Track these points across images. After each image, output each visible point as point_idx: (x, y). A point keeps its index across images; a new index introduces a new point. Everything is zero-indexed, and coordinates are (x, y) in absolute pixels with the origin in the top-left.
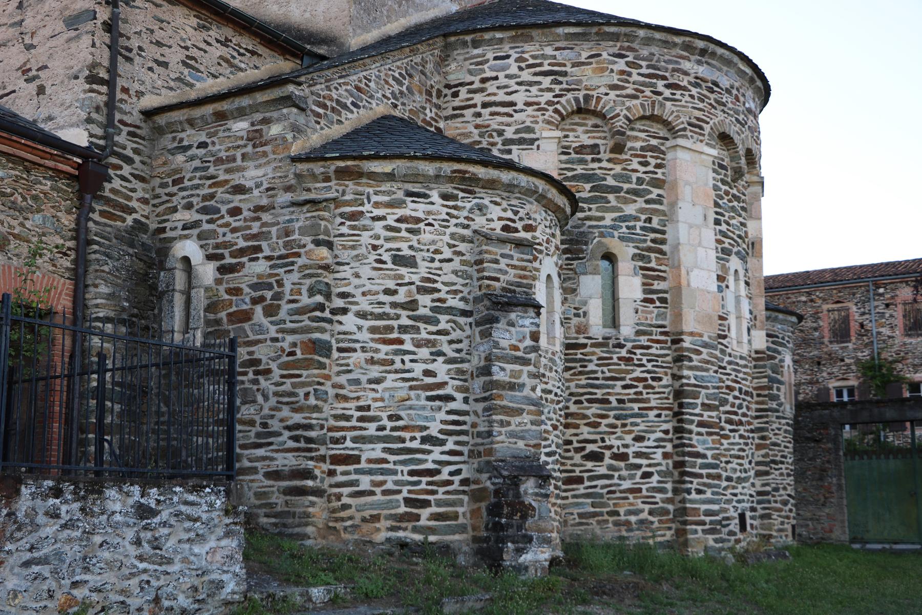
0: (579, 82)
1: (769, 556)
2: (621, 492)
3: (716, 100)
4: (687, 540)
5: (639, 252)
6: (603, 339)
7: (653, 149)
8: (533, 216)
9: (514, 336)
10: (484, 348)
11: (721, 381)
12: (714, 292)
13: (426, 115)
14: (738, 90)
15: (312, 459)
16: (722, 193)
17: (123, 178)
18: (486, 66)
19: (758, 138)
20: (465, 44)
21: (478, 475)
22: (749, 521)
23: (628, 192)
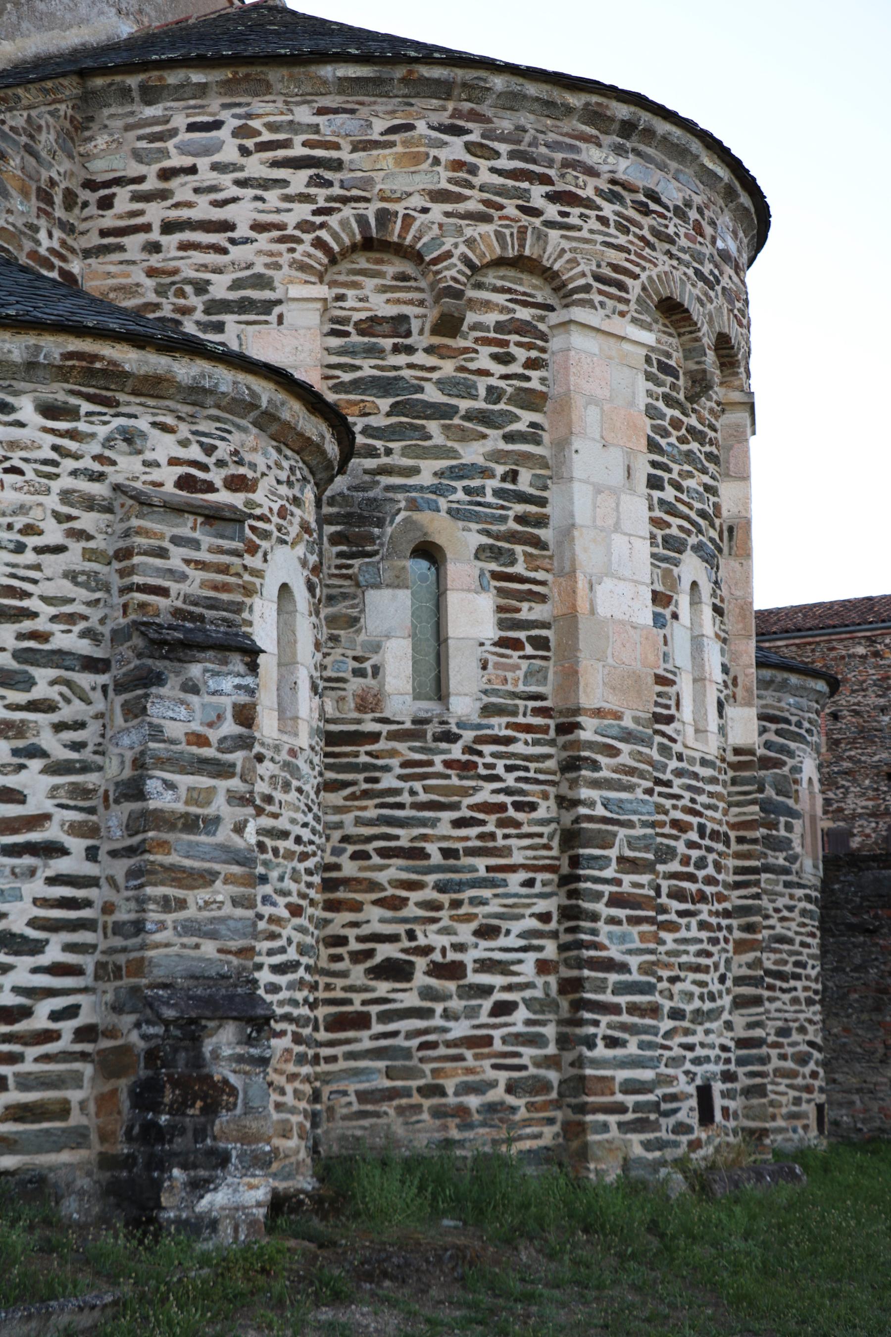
0: (367, 183)
1: (760, 1177)
2: (449, 1044)
3: (654, 231)
4: (585, 1146)
5: (490, 541)
6: (414, 722)
7: (522, 328)
8: (248, 457)
9: (198, 715)
10: (130, 741)
11: (660, 809)
12: (645, 627)
13: (38, 243)
14: (700, 211)
16: (666, 423)
18: (170, 144)
19: (743, 313)
20: (125, 94)
21: (113, 1019)
22: (718, 1102)
23: (468, 417)
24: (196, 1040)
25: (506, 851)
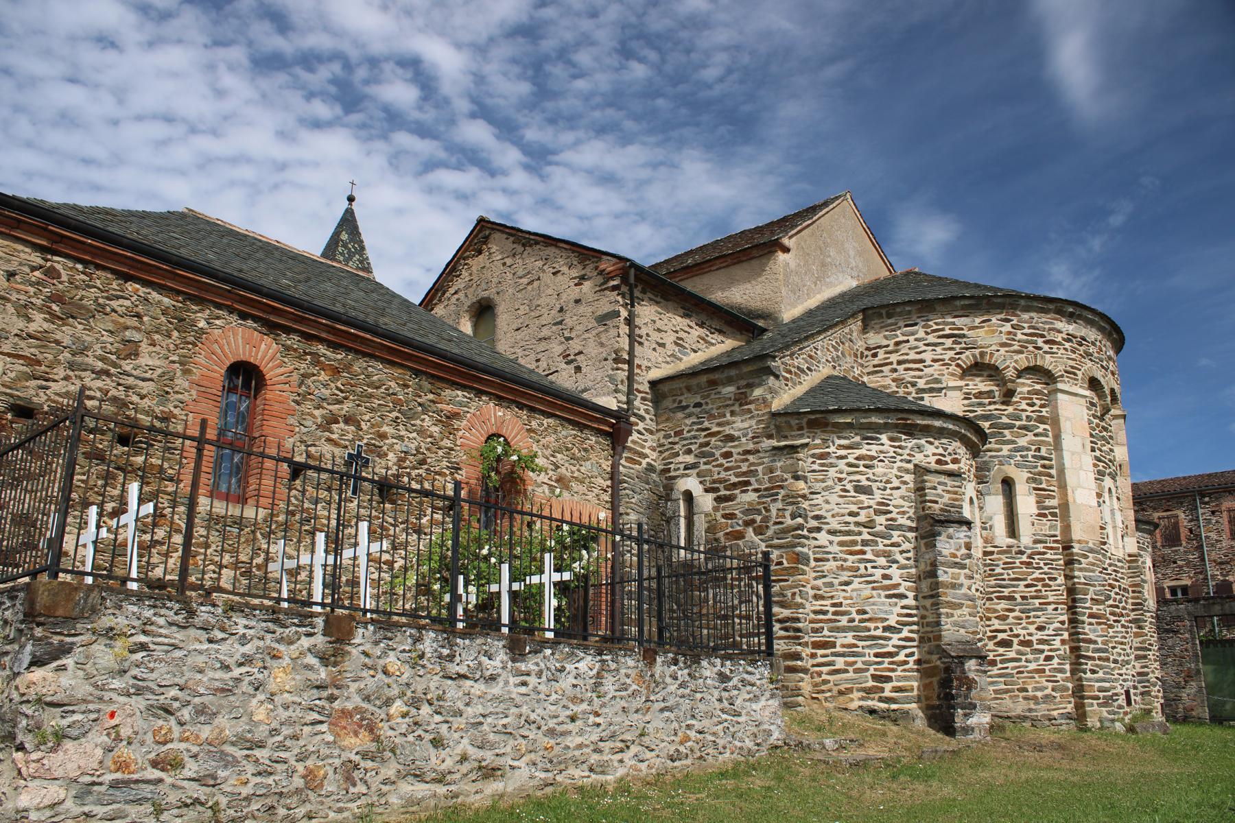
15: (800, 644)
17: (639, 432)
21: (928, 657)
22: (1133, 697)
24: (963, 664)
25: (1046, 597)
